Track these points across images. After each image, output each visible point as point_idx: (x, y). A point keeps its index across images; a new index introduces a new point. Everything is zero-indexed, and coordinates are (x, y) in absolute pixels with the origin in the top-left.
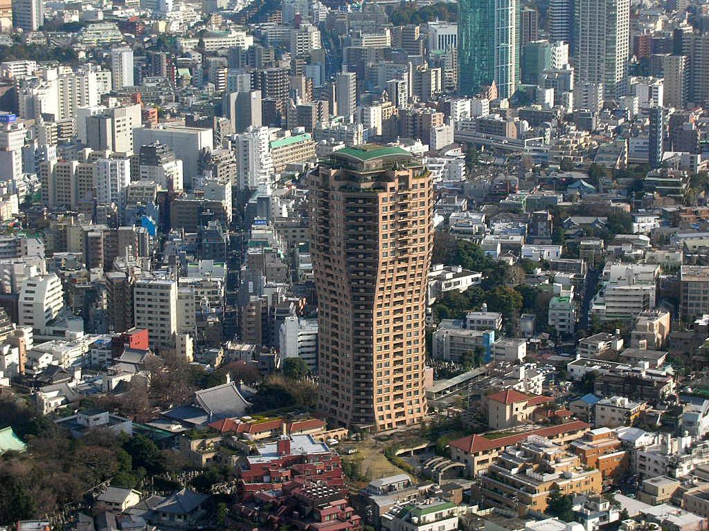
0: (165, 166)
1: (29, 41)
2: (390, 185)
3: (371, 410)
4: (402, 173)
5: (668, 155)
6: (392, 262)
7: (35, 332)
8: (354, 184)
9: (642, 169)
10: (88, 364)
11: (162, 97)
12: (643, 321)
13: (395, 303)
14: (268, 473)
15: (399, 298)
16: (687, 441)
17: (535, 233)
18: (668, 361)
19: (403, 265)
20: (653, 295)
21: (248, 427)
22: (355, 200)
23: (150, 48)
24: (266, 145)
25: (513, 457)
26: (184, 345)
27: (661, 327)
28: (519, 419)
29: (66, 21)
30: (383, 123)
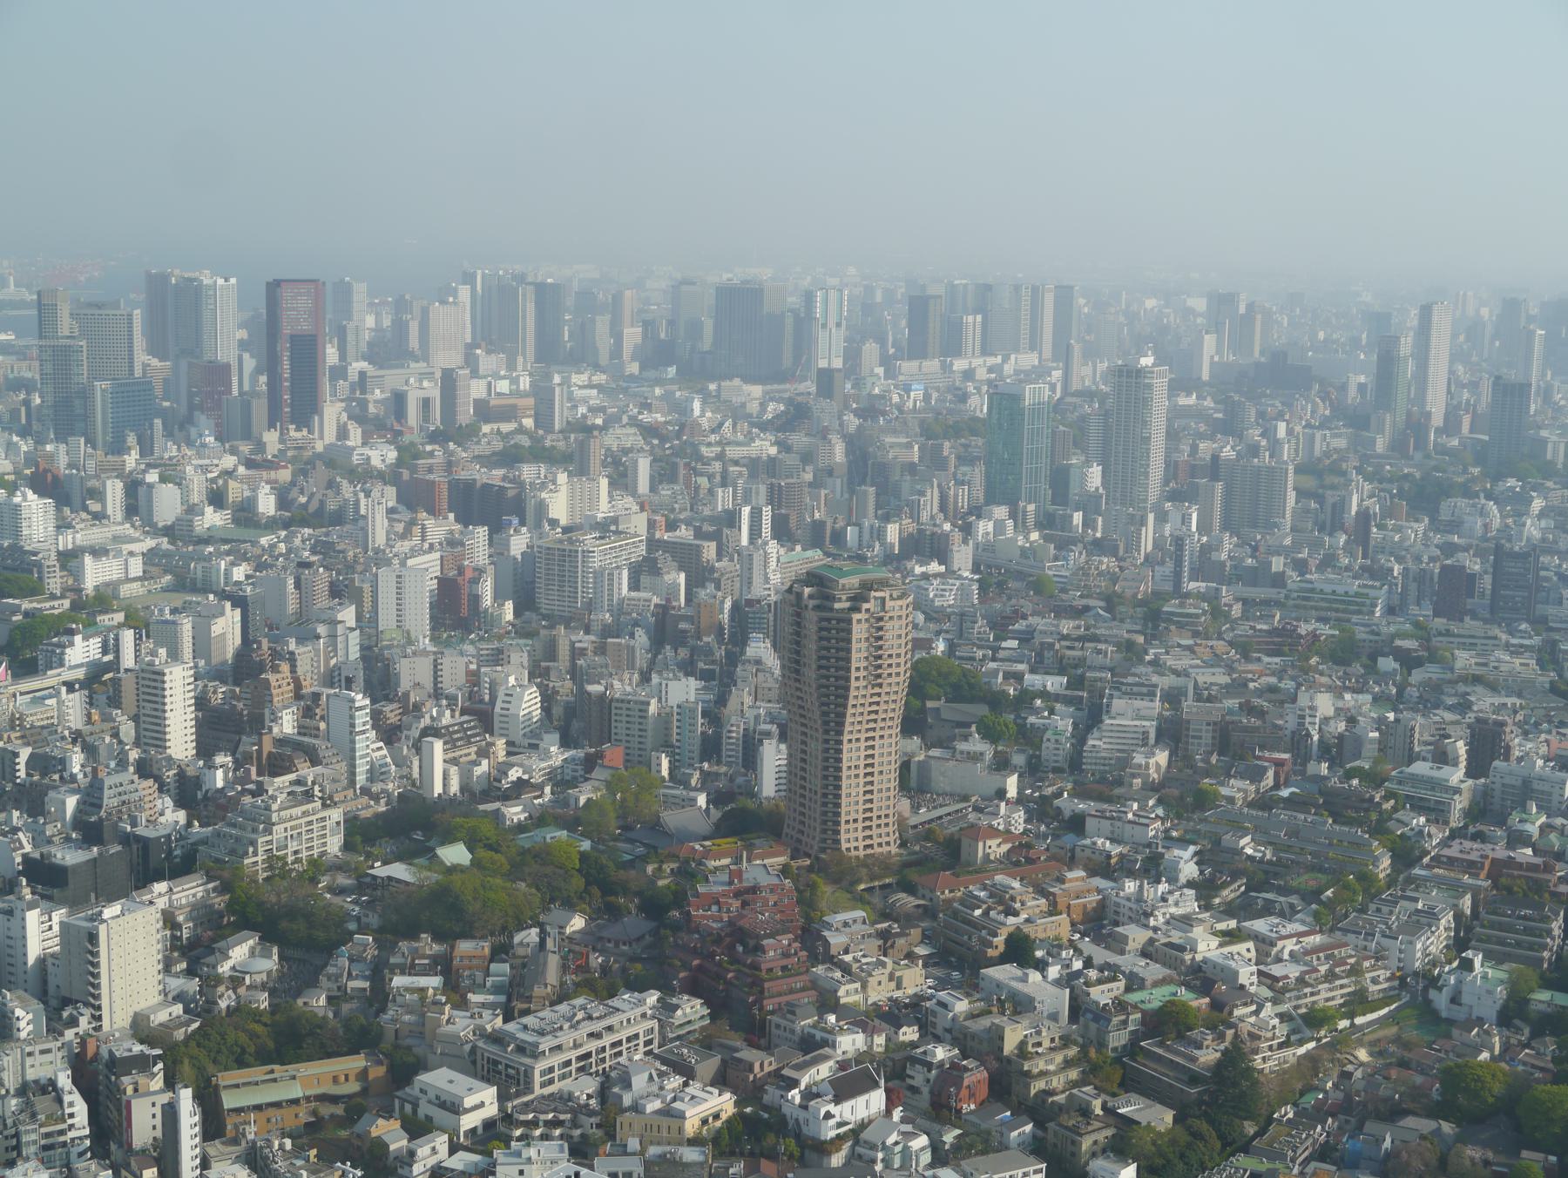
0: (666, 577)
1: (548, 443)
2: (865, 606)
3: (838, 842)
5: (1193, 585)
7: (509, 743)
8: (827, 603)
10: (562, 781)
12: (1139, 759)
13: (868, 730)
14: (718, 903)
15: (872, 725)
16: (1163, 887)
18: (1160, 802)
19: (877, 690)
21: (707, 853)
22: (829, 620)
25: (976, 897)
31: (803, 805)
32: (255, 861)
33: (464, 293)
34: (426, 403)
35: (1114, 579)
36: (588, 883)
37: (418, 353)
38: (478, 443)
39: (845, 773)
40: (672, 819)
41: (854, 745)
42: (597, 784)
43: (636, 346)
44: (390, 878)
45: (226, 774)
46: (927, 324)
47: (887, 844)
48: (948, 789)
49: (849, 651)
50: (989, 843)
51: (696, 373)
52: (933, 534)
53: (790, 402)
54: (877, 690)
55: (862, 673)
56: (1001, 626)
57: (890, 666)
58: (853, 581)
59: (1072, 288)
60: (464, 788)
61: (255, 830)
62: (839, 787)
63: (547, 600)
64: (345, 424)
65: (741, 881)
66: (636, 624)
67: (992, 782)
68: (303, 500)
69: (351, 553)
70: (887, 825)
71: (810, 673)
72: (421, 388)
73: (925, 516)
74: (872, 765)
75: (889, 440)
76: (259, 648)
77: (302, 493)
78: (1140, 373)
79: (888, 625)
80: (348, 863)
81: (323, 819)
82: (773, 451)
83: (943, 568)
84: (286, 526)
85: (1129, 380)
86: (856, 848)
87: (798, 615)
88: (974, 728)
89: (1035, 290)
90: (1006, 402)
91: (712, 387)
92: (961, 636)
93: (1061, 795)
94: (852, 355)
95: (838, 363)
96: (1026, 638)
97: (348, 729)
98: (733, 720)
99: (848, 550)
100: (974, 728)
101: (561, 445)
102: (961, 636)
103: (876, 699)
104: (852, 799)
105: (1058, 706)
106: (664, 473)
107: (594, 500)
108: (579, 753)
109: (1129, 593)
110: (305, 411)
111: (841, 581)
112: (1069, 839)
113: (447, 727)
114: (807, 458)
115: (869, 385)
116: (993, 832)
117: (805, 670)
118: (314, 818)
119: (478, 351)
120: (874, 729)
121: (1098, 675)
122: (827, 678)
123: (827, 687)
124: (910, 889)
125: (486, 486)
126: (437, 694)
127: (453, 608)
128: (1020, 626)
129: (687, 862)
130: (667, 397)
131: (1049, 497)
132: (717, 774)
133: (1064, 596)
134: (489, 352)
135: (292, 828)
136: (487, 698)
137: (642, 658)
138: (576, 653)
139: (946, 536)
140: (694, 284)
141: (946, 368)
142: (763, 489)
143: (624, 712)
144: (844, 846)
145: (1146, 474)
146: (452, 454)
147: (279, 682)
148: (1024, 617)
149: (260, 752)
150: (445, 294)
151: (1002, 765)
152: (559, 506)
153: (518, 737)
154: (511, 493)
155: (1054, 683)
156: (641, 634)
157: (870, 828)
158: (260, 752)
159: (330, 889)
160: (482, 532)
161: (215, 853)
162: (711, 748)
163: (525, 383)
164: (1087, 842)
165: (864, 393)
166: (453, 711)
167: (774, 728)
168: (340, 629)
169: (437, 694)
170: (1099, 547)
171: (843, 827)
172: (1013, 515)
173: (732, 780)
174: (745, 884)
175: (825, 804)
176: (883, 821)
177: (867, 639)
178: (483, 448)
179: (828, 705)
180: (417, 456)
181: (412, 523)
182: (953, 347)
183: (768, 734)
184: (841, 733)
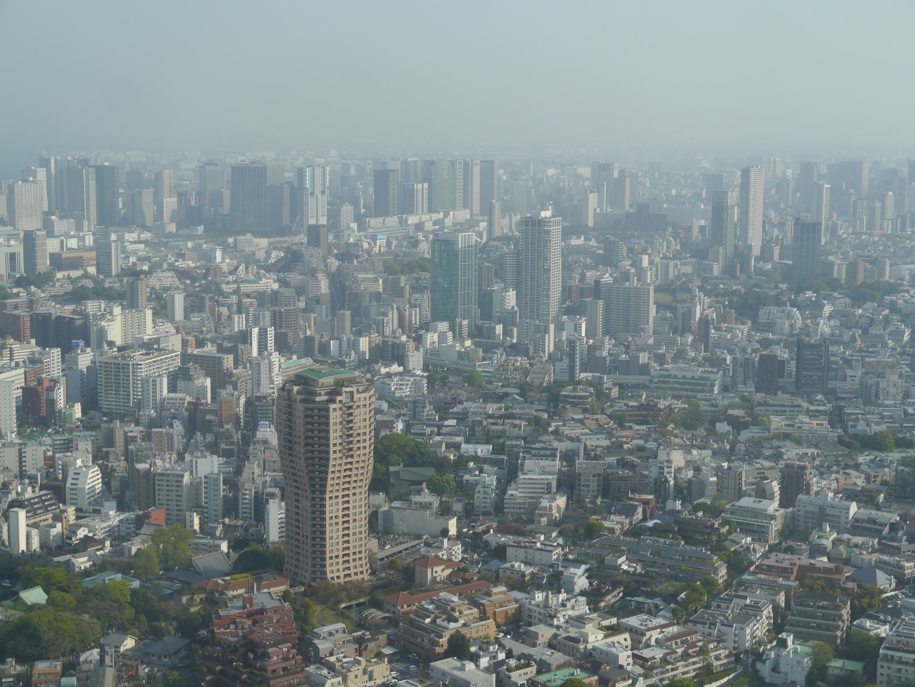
1: (107, 285)
2: (339, 398)
3: (325, 573)
4: (348, 389)
6: (341, 458)
7: (78, 510)
8: (311, 397)
9: (559, 384)
10: (118, 536)
11: (204, 329)
12: (545, 503)
13: (344, 490)
14: (235, 623)
15: (347, 486)
16: (563, 596)
17: (473, 435)
19: (350, 460)
20: (554, 485)
21: (227, 586)
22: (312, 409)
23: (200, 291)
24: (277, 366)
25: (427, 610)
26: (192, 521)
27: (559, 507)
28: (438, 580)
29: (138, 269)
35: (526, 372)
36: (137, 613)
38: (54, 286)
39: (328, 522)
41: (334, 501)
42: (144, 537)
43: (173, 211)
46: (388, 190)
47: (360, 572)
48: (406, 530)
49: (328, 432)
50: (435, 569)
51: (219, 230)
52: (394, 344)
53: (288, 250)
54: (350, 460)
55: (338, 448)
56: (443, 409)
57: (359, 441)
58: (329, 380)
59: (493, 162)
62: (324, 533)
65: (251, 605)
66: (174, 417)
70: (360, 559)
71: (300, 449)
73: (388, 331)
74: (348, 515)
75: (361, 276)
78: (541, 222)
79: (356, 412)
82: (276, 286)
83: (401, 369)
85: (534, 228)
86: (338, 577)
87: (290, 406)
88: (424, 485)
89: (466, 164)
92: (414, 418)
94: (334, 215)
95: (323, 221)
96: (462, 418)
98: (247, 486)
100: (424, 485)
101: (117, 286)
102: (414, 418)
103: (349, 466)
104: (334, 541)
105: (486, 467)
106: (194, 305)
107: (142, 326)
108: (131, 515)
109: (537, 382)
111: (321, 381)
112: (494, 564)
113: (29, 500)
114: (300, 291)
115: (346, 236)
116: (438, 561)
117: (296, 447)
119: (53, 217)
120: (348, 489)
121: (514, 443)
123: (313, 459)
124: (378, 605)
125: (59, 318)
128: (458, 409)
129: (212, 592)
132: (236, 526)
133: (490, 386)
136: (60, 476)
139: (403, 345)
140: (216, 164)
141: (403, 222)
142: (268, 314)
143: (165, 483)
144: (329, 576)
146: (33, 294)
148: (461, 403)
150: (26, 175)
151: (445, 511)
153: (84, 504)
154: (78, 323)
155: (483, 450)
157: (348, 561)
160: (56, 352)
162: (230, 507)
163: (89, 240)
165: (343, 242)
166: (33, 487)
170: (515, 349)
171: (328, 562)
172: (452, 328)
173: (246, 530)
174: (255, 608)
175: (314, 546)
176: (357, 556)
177: (341, 423)
178: (57, 290)
179: (314, 472)
182: (408, 207)
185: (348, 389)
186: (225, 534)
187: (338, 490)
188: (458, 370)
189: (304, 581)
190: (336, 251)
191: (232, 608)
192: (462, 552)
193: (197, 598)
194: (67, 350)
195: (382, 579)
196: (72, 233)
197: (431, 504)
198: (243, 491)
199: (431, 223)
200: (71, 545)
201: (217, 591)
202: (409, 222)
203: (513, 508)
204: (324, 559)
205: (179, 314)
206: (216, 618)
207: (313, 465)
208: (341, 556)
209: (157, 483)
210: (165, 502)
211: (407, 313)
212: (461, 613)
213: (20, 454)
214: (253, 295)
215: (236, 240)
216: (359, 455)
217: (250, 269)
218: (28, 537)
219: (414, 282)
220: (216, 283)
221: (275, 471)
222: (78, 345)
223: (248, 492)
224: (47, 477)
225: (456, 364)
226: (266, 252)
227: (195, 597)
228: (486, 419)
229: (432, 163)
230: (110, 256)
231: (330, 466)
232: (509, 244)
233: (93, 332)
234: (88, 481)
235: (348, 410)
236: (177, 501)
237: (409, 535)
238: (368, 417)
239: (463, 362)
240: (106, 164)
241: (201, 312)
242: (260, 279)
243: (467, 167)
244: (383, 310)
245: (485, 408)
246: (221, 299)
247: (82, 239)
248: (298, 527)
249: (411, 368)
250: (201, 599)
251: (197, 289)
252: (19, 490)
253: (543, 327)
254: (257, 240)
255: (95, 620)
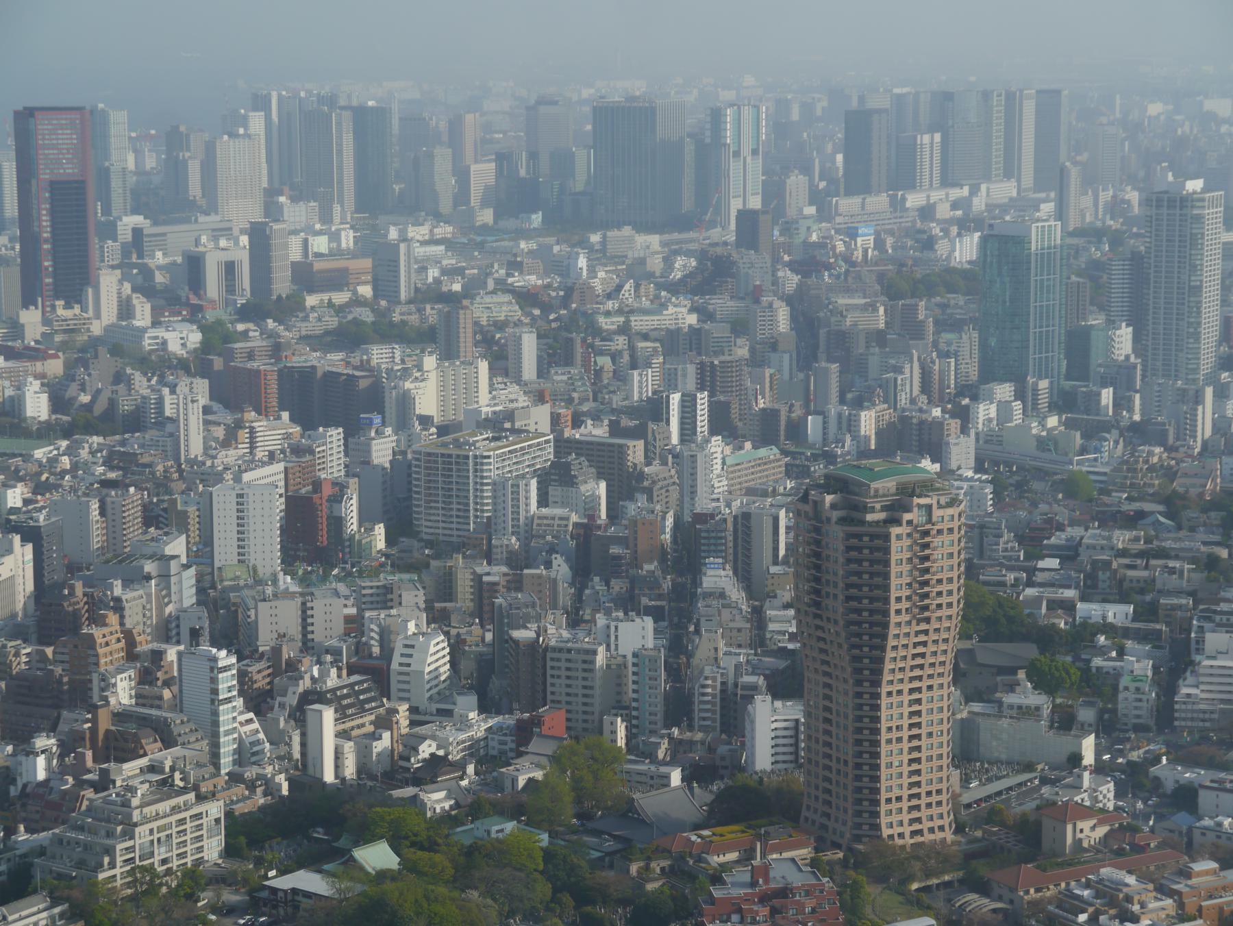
1: (396, 317)
2: (907, 517)
3: (877, 827)
4: (923, 501)
6: (909, 623)
7: (413, 710)
10: (489, 757)
11: (575, 395)
13: (912, 679)
14: (739, 910)
15: (917, 672)
17: (1095, 586)
19: (923, 626)
21: (708, 846)
22: (859, 536)
24: (719, 461)
25: (1079, 898)
26: (614, 732)
28: (1085, 845)
29: (445, 289)
30: (879, 433)
31: (829, 780)
32: (114, 874)
33: (257, 122)
34: (230, 269)
35: (1170, 474)
36: (556, 890)
37: (203, 203)
38: (306, 319)
39: (884, 736)
40: (649, 803)
41: (895, 699)
42: (536, 759)
43: (487, 188)
44: (295, 891)
45: (49, 761)
46: (871, 147)
47: (938, 828)
48: (1004, 757)
49: (887, 576)
50: (1080, 825)
51: (572, 219)
52: (922, 423)
53: (702, 256)
54: (923, 626)
55: (905, 605)
56: (1033, 540)
57: (940, 594)
58: (887, 485)
59: (1058, 92)
60: (362, 769)
61: (110, 834)
62: (877, 755)
63: (428, 522)
64: (129, 298)
65: (767, 881)
66: (552, 550)
67: (1059, 745)
68: (85, 398)
69: (160, 468)
70: (939, 803)
71: (836, 606)
72: (227, 250)
73: (903, 399)
74: (919, 725)
75: (842, 301)
76: (72, 594)
77: (83, 389)
78: (1186, 201)
79: (937, 541)
80: (234, 873)
81: (198, 816)
82: (692, 319)
83: (937, 467)
84: (67, 434)
85: (1172, 212)
86: (901, 835)
87: (817, 530)
88: (1021, 675)
89: (1010, 97)
90: (1005, 248)
91: (595, 238)
92: (981, 555)
93: (1157, 760)
94: (774, 192)
95: (755, 203)
96: (1069, 554)
97: (208, 697)
98: (708, 671)
99: (812, 447)
100: (1021, 675)
101: (414, 319)
102: (981, 555)
103: (922, 638)
104: (894, 771)
105: (1129, 644)
106: (556, 353)
107: (471, 389)
108: (509, 720)
109: (1193, 492)
110: (74, 282)
111: (874, 485)
112: (1181, 819)
113: (334, 690)
114: (740, 327)
115: (803, 231)
116: (1084, 812)
118: (187, 814)
119: (282, 199)
120: (920, 678)
121: (1175, 601)
122: (858, 611)
123: (859, 624)
124: (983, 889)
125: (330, 376)
126: (308, 646)
127: (309, 534)
128: (1057, 539)
129: (682, 857)
130: (542, 253)
131: (1064, 369)
132: (692, 743)
133: (1105, 499)
134: (294, 200)
135: (160, 830)
136: (376, 650)
137: (565, 593)
138: (483, 590)
139: (939, 425)
140: (556, 103)
141: (897, 205)
142: (691, 369)
143: (563, 664)
144: (886, 832)
145: (1197, 336)
146: (272, 335)
147: (106, 638)
148: (1061, 528)
149: (94, 730)
150: (232, 124)
151: (1065, 722)
152: (427, 399)
153: (423, 702)
154: (363, 384)
155: (1118, 613)
156: (559, 561)
157: (918, 808)
158: (94, 730)
159: (214, 909)
160: (335, 435)
161: (57, 867)
162: (679, 708)
163: (348, 239)
164: (1207, 822)
165: (798, 240)
166: (339, 669)
167: (761, 681)
168: (174, 566)
169: (308, 646)
170: (1139, 433)
171: (884, 808)
172: (1020, 395)
173: (711, 750)
174: (772, 885)
175: (858, 778)
176: (934, 798)
177: (910, 560)
178: (312, 326)
179: (860, 647)
180: (228, 338)
181: (239, 425)
182: (904, 176)
183: (754, 688)
184: (878, 683)
185: (923, 501)
186: (673, 757)
187: (901, 681)
188: (1039, 469)
189: (841, 841)
190: (786, 258)
191: (734, 884)
192: (1116, 797)
193: (656, 866)
194: (354, 431)
195: (977, 840)
196: (318, 226)
197: (1038, 708)
198: (702, 681)
199: (948, 205)
200: (409, 769)
201: (691, 855)
202: (908, 204)
203: (1192, 719)
204: (877, 803)
205: (529, 369)
206: (706, 902)
207: (859, 635)
208: (905, 797)
209: (549, 664)
210: (564, 698)
211: (936, 367)
212: (1143, 905)
213: (304, 612)
214: (653, 335)
215: (604, 237)
216: (940, 619)
217: (642, 290)
218: (338, 755)
219: (938, 311)
220: (585, 314)
221: (740, 646)
222: (370, 423)
223: (710, 688)
224: (357, 652)
225: (1035, 459)
226: (665, 259)
227: (653, 865)
228: (1116, 557)
229: (948, 96)
230: (398, 266)
231: (890, 637)
232: (1100, 241)
233: (391, 398)
234: (430, 660)
235: (922, 538)
236: (585, 696)
237: (1008, 763)
238: (955, 549)
239: (1045, 455)
240: (370, 103)
241: (567, 365)
242: (664, 306)
243: (1012, 100)
244: (893, 362)
245: (1109, 538)
246: (598, 343)
247: (335, 237)
248: (829, 745)
249: (954, 466)
250: (663, 869)
251: (554, 325)
252: (316, 673)
253: (1191, 393)
254: (641, 239)
255: (489, 901)
